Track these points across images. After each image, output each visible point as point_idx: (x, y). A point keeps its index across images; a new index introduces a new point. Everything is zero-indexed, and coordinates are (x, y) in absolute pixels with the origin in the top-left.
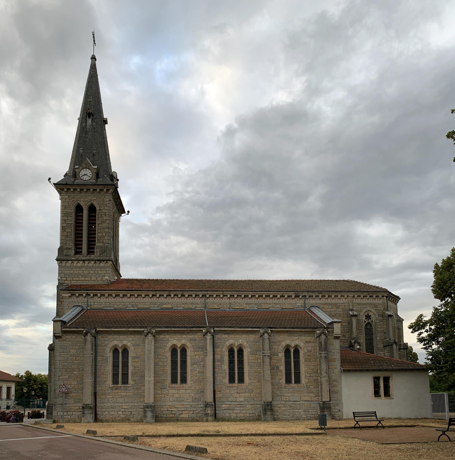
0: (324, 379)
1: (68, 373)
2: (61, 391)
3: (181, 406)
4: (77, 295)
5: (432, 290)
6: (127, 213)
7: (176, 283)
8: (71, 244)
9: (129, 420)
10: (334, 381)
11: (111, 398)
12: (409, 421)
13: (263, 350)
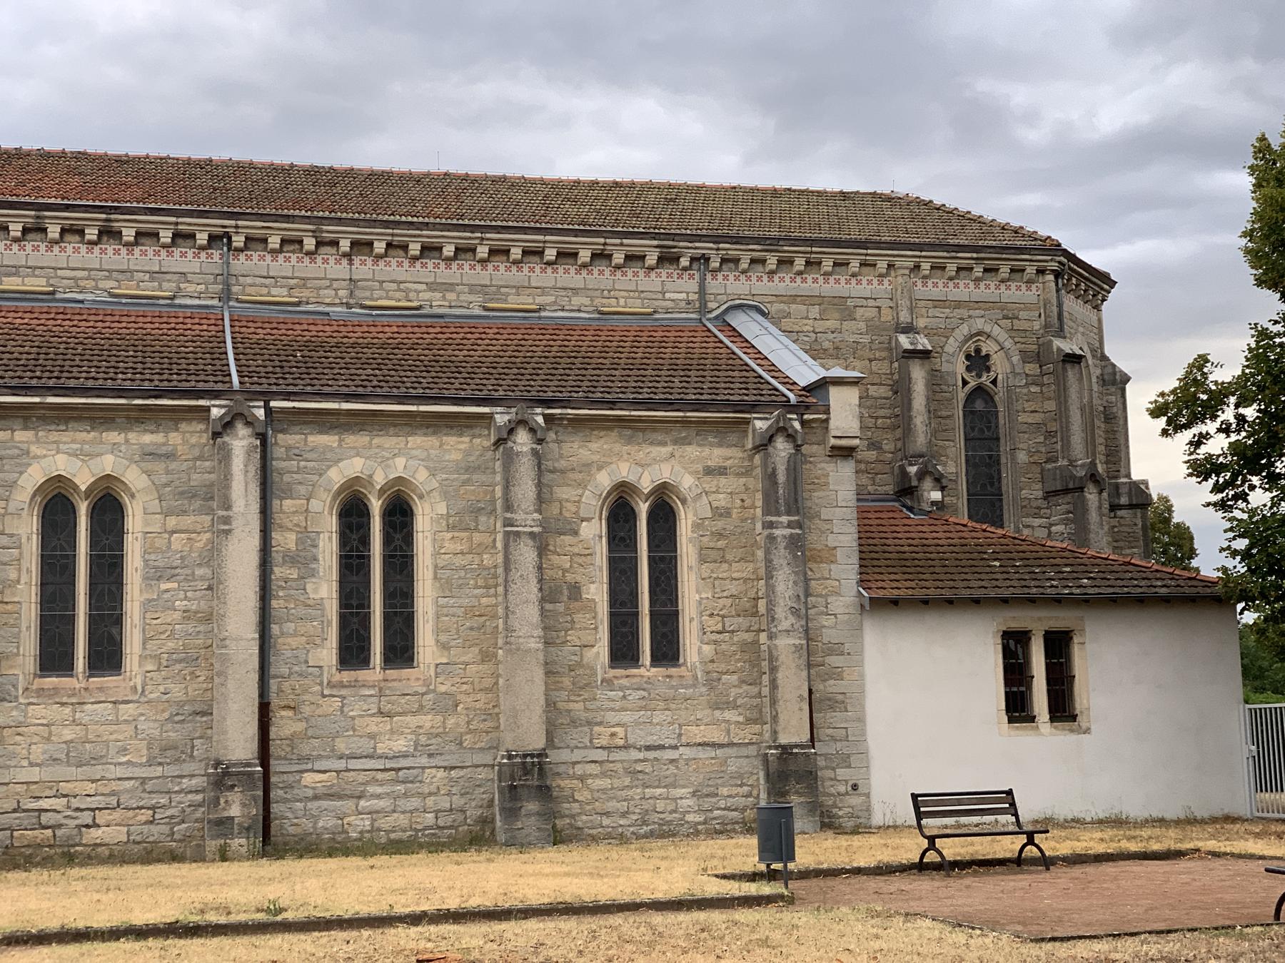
3: (91, 788)
5: (1247, 251)
7: (71, 172)
12: (1157, 831)
13: (508, 507)
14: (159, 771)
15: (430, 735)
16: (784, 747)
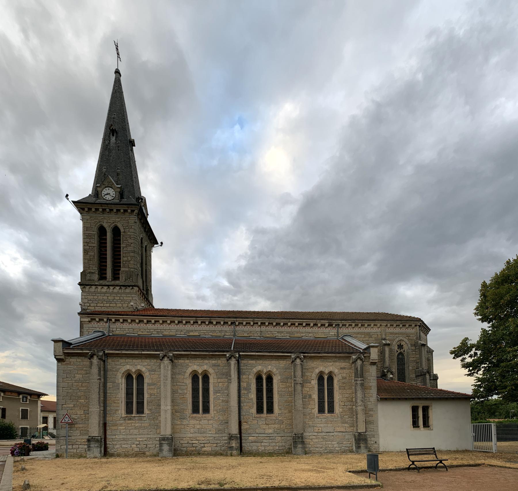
0: (359, 408)
1: (72, 402)
2: (63, 421)
3: (203, 439)
4: (97, 319)
6: (160, 244)
8: (95, 269)
9: (144, 453)
10: (370, 411)
11: (123, 429)
13: (295, 377)
14: (218, 435)
15: (277, 429)
16: (359, 433)
